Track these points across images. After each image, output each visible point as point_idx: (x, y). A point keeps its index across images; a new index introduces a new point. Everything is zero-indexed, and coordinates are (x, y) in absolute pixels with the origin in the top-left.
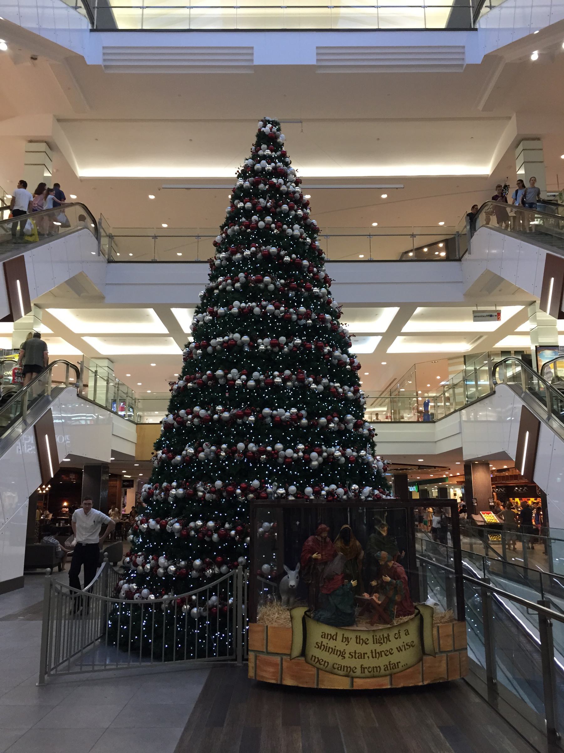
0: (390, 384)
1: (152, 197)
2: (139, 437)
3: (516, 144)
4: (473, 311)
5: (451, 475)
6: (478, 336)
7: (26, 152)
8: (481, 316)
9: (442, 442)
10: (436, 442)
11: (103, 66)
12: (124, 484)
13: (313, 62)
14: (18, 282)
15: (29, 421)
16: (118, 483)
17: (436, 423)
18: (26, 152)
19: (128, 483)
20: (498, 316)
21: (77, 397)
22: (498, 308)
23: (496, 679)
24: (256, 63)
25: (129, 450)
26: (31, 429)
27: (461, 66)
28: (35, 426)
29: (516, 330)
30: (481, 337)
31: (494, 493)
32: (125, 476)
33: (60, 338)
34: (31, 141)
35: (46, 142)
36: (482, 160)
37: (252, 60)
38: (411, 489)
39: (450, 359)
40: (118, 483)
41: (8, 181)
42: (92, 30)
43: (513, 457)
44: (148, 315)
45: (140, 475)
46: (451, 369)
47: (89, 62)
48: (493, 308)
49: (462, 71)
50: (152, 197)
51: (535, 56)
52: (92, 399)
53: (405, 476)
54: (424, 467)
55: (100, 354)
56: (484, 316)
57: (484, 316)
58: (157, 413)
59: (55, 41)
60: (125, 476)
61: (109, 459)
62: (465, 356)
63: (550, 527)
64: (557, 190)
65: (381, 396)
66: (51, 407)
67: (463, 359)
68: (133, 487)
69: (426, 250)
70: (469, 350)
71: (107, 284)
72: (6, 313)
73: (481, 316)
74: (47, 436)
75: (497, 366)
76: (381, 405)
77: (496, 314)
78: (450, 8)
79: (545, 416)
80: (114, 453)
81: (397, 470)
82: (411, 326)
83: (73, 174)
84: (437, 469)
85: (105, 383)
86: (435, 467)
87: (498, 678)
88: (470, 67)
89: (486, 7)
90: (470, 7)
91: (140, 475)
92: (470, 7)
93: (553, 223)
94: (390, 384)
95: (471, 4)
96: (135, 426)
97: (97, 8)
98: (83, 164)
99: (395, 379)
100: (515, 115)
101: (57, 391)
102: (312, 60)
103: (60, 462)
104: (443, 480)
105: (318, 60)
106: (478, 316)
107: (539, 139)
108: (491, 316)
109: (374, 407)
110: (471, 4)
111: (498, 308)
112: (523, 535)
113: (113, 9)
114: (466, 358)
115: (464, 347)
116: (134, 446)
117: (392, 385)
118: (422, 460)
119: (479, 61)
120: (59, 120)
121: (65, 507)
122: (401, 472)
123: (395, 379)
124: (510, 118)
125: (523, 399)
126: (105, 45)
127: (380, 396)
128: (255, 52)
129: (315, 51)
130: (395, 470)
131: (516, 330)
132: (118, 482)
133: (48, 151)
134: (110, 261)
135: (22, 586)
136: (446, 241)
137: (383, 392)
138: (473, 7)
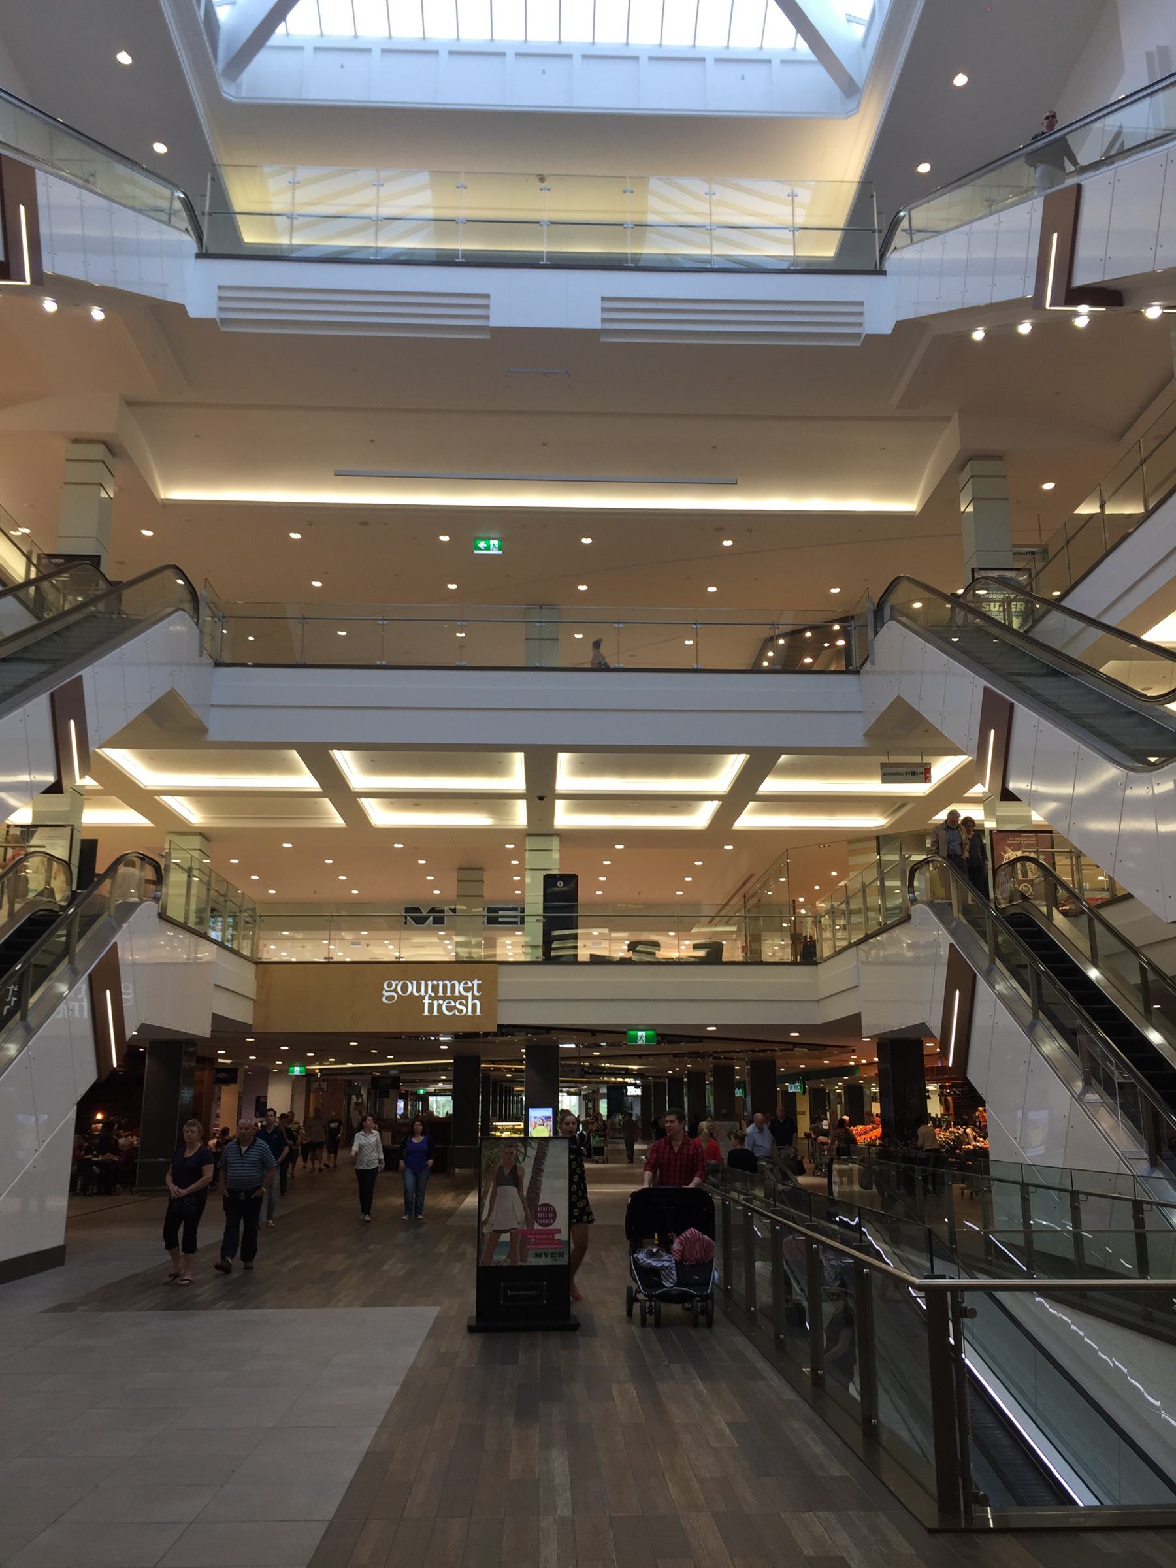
0: (744, 884)
1: (296, 536)
2: (260, 987)
3: (963, 461)
4: (882, 764)
5: (864, 1061)
6: (899, 804)
7: (68, 460)
8: (896, 774)
9: (829, 1001)
10: (818, 1001)
11: (218, 320)
12: (218, 1076)
13: (597, 324)
14: (72, 723)
15: (79, 965)
16: (207, 1075)
17: (819, 966)
18: (68, 460)
19: (226, 1075)
20: (926, 774)
21: (157, 919)
22: (926, 759)
23: (876, 1417)
24: (493, 323)
25: (242, 1013)
26: (84, 979)
27: (858, 335)
28: (90, 976)
29: (967, 795)
30: (903, 805)
31: (949, 1098)
32: (220, 1060)
33: (115, 798)
34: (76, 441)
35: (104, 443)
36: (900, 489)
37: (487, 317)
38: (791, 1088)
39: (850, 842)
40: (207, 1075)
41: (26, 505)
42: (199, 256)
43: (937, 1033)
44: (285, 760)
45: (251, 1058)
46: (853, 860)
47: (193, 312)
48: (916, 759)
49: (859, 345)
50: (296, 536)
51: (978, 335)
52: (182, 920)
53: (771, 1065)
54: (816, 1047)
55: (187, 825)
56: (900, 774)
57: (900, 774)
58: (285, 933)
59: (139, 292)
60: (220, 1060)
61: (203, 1029)
62: (878, 838)
63: (991, 1158)
64: (1038, 542)
65: (721, 914)
66: (117, 938)
67: (874, 843)
68: (235, 1082)
69: (808, 634)
70: (927, 793)
71: (212, 706)
72: (50, 778)
73: (896, 774)
74: (108, 992)
75: (916, 869)
76: (727, 924)
77: (922, 770)
78: (841, 231)
79: (985, 964)
80: (216, 1019)
81: (753, 1051)
82: (771, 785)
83: (149, 495)
84: (829, 1050)
85: (184, 876)
86: (825, 1047)
87: (881, 1416)
88: (874, 340)
89: (902, 230)
90: (874, 231)
91: (251, 1058)
92: (874, 231)
93: (1023, 610)
94: (744, 884)
95: (876, 227)
96: (254, 966)
97: (210, 214)
98: (174, 479)
99: (752, 876)
100: (957, 413)
101: (128, 909)
102: (592, 321)
103: (128, 1038)
104: (850, 1071)
105: (604, 320)
106: (890, 774)
107: (999, 457)
108: (913, 773)
109: (716, 926)
110: (876, 227)
111: (926, 759)
112: (983, 1179)
113: (238, 216)
114: (880, 840)
115: (874, 821)
116: (251, 1004)
117: (749, 884)
118: (797, 1034)
119: (887, 329)
120: (130, 404)
121: (99, 1121)
122: (762, 1054)
123: (752, 876)
124: (949, 419)
125: (953, 933)
126: (222, 284)
127: (718, 913)
128: (492, 302)
129: (599, 304)
130: (751, 1051)
131: (967, 795)
132: (206, 1073)
133: (109, 460)
134: (218, 664)
135: (62, 1264)
136: (844, 620)
137: (725, 906)
138: (880, 231)
